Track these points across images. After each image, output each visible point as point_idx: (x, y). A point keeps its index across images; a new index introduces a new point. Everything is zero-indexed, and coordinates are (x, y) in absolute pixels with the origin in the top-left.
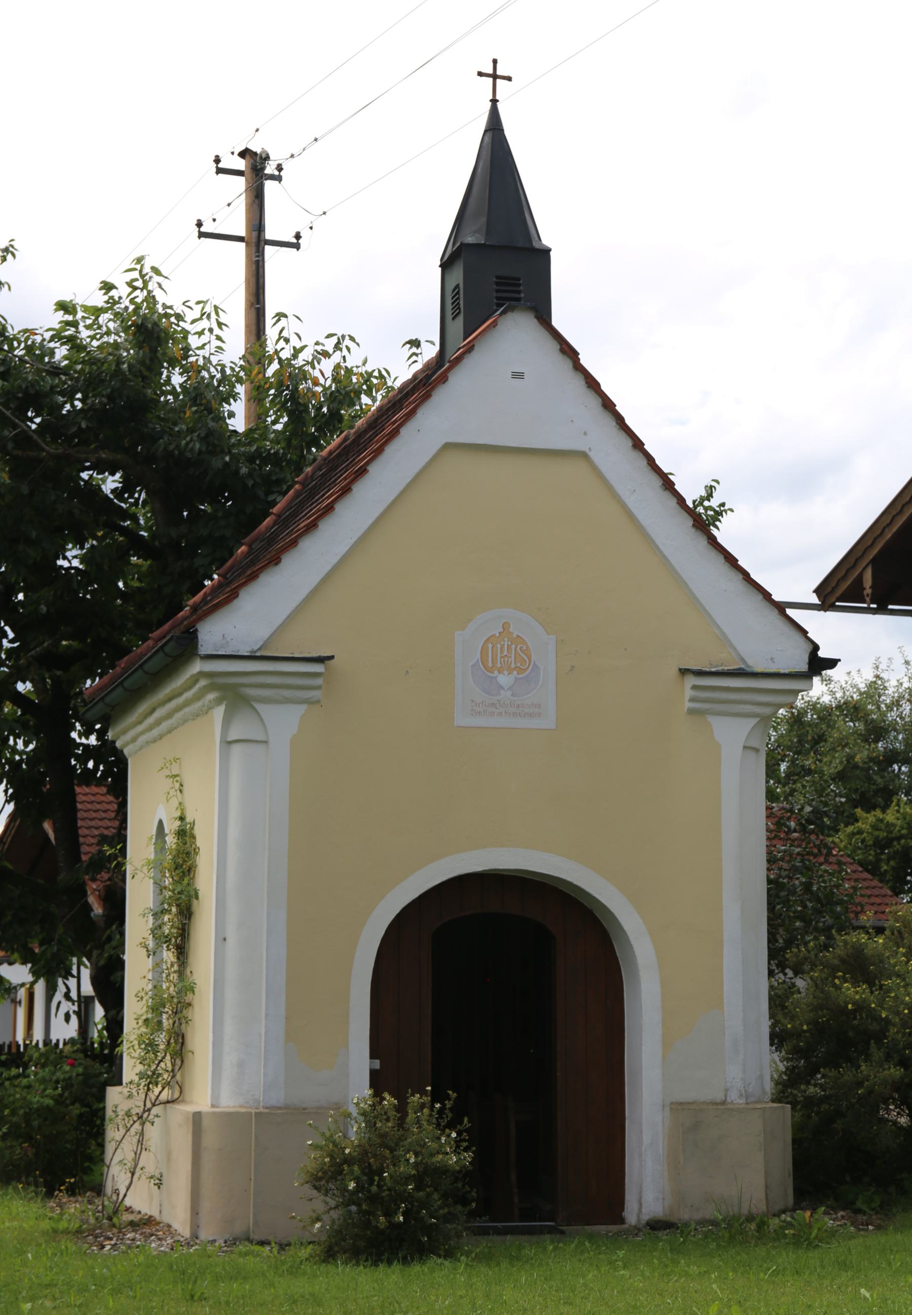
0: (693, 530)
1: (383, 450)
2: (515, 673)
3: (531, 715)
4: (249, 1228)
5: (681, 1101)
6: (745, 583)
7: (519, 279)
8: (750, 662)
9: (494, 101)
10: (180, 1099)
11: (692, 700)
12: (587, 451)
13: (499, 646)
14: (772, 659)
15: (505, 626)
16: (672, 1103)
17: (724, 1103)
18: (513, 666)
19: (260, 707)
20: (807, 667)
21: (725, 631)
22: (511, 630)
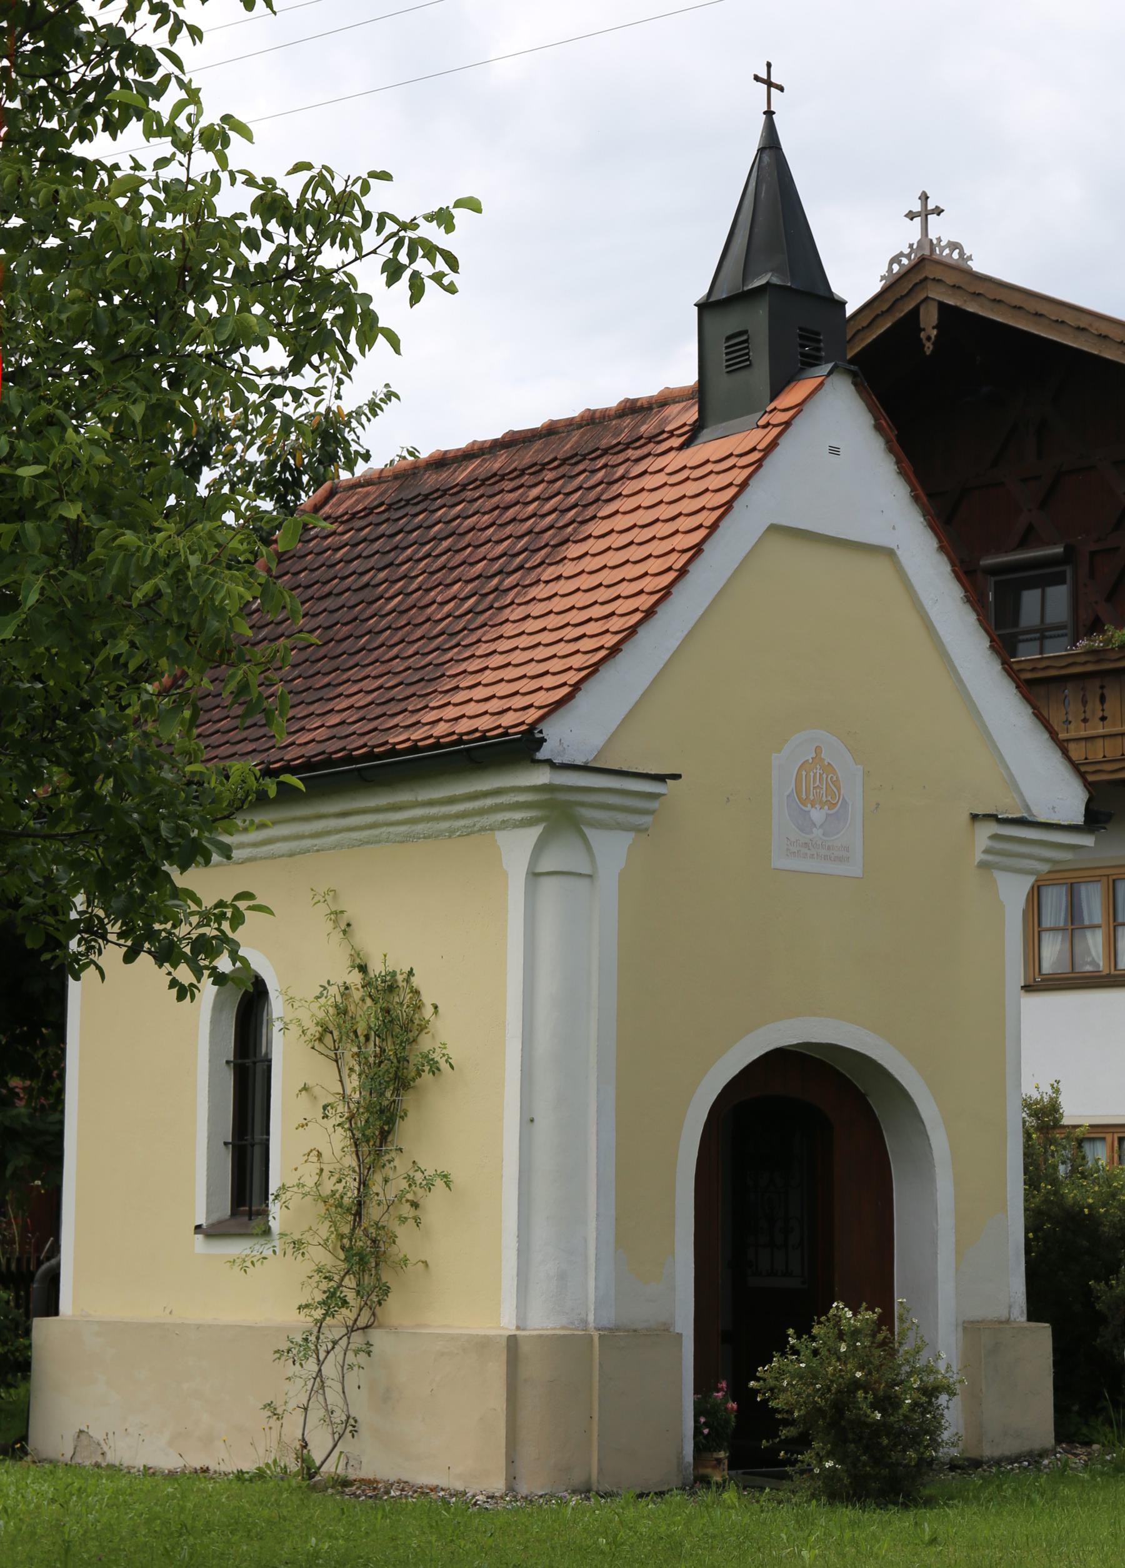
0: (989, 652)
1: (718, 526)
2: (826, 807)
3: (840, 859)
4: (590, 1477)
5: (972, 1319)
6: (1034, 718)
7: (818, 334)
8: (1035, 810)
9: (769, 113)
10: (375, 1323)
11: (986, 852)
12: (895, 548)
13: (812, 774)
14: (1054, 808)
15: (818, 750)
16: (964, 1322)
17: (1008, 1321)
18: (824, 799)
19: (590, 832)
20: (1083, 819)
21: (1014, 772)
22: (823, 756)
